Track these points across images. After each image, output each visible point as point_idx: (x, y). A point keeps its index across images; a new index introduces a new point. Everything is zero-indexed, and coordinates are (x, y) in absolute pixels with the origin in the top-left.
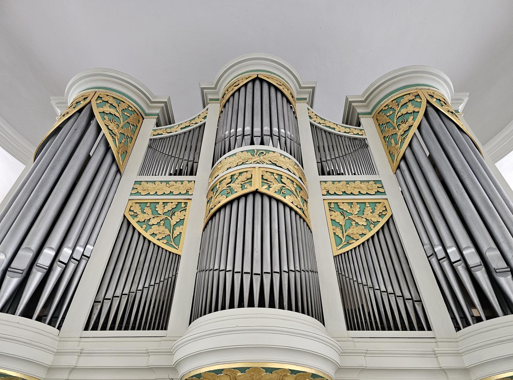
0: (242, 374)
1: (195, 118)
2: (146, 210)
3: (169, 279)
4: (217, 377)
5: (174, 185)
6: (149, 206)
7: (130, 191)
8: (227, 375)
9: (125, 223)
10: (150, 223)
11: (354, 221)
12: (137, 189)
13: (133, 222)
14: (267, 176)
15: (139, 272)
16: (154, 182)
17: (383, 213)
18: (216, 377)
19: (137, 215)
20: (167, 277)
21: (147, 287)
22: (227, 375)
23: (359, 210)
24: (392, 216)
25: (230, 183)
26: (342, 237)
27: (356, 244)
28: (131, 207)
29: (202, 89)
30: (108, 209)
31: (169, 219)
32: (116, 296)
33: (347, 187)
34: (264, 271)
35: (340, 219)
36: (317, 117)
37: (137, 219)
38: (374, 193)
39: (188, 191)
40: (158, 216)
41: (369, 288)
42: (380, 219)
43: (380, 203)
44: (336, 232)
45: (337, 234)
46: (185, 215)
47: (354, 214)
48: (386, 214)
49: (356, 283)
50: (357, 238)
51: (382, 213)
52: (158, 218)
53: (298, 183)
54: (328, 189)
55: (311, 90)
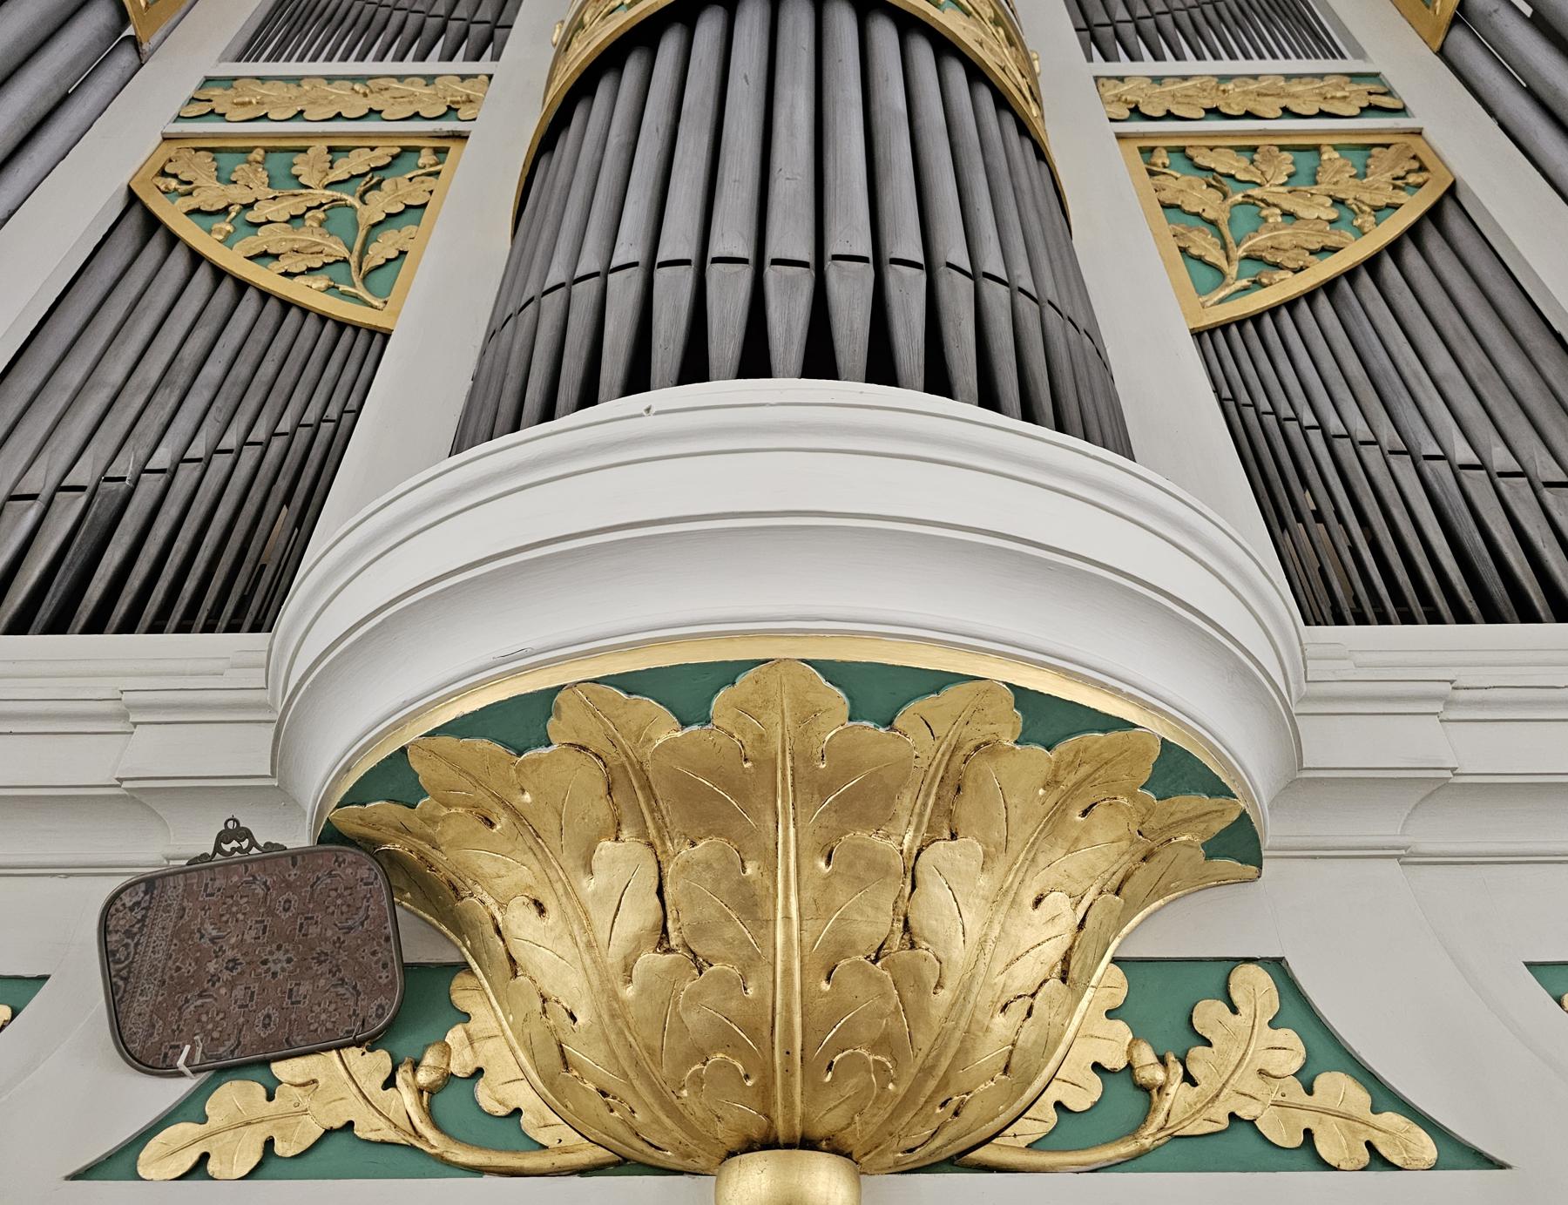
0: (687, 730)
2: (239, 173)
3: (323, 425)
4: (518, 771)
5: (386, 89)
6: (259, 158)
7: (176, 105)
8: (585, 749)
9: (134, 218)
10: (251, 216)
11: (1275, 205)
12: (209, 101)
13: (172, 214)
15: (167, 399)
16: (297, 80)
17: (1412, 179)
18: (513, 773)
19: (194, 189)
20: (311, 416)
21: (198, 456)
22: (585, 749)
23: (1292, 169)
24: (1452, 191)
26: (1223, 263)
28: (171, 161)
30: (53, 163)
31: (352, 207)
32: (25, 492)
33: (1224, 91)
34: (834, 247)
35: (1199, 197)
38: (1357, 111)
39: (453, 106)
40: (296, 192)
41: (1391, 452)
43: (1387, 146)
44: (1190, 244)
45: (1194, 251)
46: (431, 192)
47: (1272, 182)
48: (1425, 182)
49: (1316, 437)
50: (1301, 263)
51: (1403, 178)
52: (298, 199)
54: (1135, 99)
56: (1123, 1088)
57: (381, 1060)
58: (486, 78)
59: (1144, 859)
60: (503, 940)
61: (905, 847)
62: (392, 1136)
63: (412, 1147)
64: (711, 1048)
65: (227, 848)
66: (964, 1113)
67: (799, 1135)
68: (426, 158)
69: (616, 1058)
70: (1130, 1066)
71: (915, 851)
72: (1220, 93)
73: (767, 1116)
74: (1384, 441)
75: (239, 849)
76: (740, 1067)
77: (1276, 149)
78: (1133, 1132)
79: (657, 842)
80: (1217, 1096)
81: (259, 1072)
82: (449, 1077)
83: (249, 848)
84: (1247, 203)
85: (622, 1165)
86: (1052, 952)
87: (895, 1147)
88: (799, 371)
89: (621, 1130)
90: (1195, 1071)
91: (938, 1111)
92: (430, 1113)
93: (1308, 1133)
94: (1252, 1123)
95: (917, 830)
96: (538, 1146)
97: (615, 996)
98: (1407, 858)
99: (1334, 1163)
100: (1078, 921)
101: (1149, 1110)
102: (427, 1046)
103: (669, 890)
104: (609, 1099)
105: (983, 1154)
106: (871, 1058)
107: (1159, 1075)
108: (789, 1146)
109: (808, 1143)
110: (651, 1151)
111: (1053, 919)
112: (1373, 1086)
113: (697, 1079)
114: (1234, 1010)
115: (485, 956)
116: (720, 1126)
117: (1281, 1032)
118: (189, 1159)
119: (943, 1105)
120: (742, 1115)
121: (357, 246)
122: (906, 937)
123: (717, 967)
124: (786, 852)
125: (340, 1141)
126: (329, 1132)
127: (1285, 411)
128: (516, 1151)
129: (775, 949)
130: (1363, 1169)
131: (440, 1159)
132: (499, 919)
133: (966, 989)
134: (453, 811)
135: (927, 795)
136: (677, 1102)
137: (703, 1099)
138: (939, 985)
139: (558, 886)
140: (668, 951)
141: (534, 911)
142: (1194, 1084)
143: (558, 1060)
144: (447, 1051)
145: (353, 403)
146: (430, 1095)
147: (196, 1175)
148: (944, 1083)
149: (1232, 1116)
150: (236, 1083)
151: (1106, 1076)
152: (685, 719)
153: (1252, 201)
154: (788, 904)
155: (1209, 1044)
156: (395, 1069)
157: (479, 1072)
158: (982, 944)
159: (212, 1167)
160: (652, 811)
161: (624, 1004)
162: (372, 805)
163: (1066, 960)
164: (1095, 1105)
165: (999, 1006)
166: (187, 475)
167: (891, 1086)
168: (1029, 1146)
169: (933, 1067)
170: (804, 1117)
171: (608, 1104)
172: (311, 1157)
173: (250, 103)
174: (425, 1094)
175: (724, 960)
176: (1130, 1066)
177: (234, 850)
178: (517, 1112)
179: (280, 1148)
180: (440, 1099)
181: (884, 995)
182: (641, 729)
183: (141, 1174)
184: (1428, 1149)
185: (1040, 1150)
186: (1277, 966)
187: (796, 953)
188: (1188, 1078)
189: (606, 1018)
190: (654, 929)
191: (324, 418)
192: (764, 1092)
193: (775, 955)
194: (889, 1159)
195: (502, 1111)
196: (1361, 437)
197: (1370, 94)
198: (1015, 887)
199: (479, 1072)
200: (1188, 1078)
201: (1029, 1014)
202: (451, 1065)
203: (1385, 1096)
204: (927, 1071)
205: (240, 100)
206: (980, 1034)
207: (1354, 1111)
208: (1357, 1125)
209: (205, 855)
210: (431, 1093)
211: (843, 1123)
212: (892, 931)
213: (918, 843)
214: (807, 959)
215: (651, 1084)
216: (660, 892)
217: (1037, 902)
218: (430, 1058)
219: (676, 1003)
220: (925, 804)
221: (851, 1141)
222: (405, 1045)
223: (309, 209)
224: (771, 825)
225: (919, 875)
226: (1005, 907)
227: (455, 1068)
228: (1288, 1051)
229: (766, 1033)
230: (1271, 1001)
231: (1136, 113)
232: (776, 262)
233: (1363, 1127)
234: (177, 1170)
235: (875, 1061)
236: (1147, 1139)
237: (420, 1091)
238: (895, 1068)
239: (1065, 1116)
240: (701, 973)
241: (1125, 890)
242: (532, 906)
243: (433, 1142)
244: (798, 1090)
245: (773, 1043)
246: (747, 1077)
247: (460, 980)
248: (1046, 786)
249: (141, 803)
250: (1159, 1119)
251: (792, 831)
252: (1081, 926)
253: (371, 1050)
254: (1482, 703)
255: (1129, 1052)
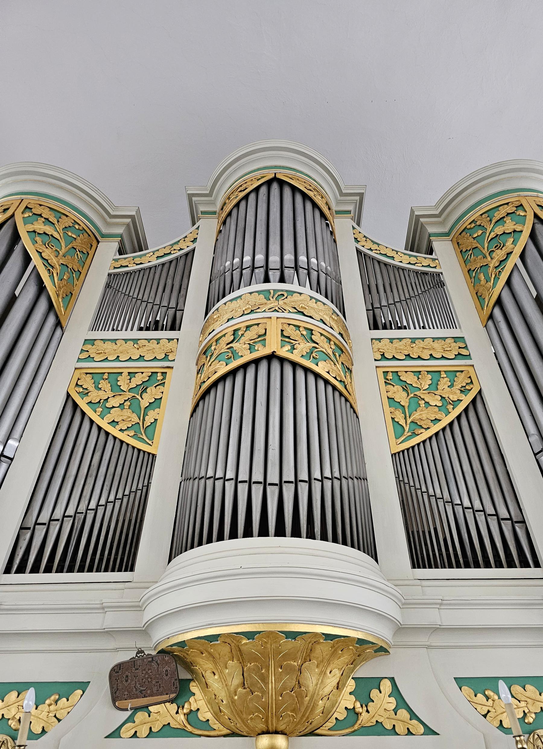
1: (179, 241)
6: (107, 377)
9: (70, 404)
12: (88, 351)
13: (82, 403)
14: (290, 331)
15: (90, 481)
16: (115, 341)
22: (226, 643)
24: (480, 392)
25: (232, 342)
26: (404, 425)
27: (426, 435)
29: (190, 196)
33: (412, 347)
36: (367, 240)
37: (87, 399)
42: (462, 397)
43: (462, 371)
45: (396, 420)
46: (162, 393)
47: (423, 389)
48: (472, 389)
49: (425, 496)
50: (428, 426)
51: (465, 387)
53: (337, 342)
54: (383, 351)
55: (358, 198)
56: (352, 713)
57: (174, 707)
58: (176, 340)
59: (358, 656)
60: (204, 679)
61: (299, 664)
62: (179, 727)
63: (184, 729)
64: (255, 712)
65: (138, 655)
66: (312, 724)
67: (274, 731)
68: (160, 377)
69: (233, 712)
70: (354, 708)
71: (301, 665)
72: (411, 348)
73: (267, 727)
74: (445, 498)
75: (141, 656)
76: (261, 716)
77: (426, 373)
78: (353, 726)
79: (242, 663)
80: (374, 716)
81: (145, 709)
82: (191, 711)
83: (144, 655)
84: (415, 397)
85: (233, 734)
86: (334, 683)
87: (296, 732)
88: (274, 536)
89: (234, 727)
90: (369, 709)
91: (306, 724)
92: (187, 720)
93: (394, 726)
94: (381, 723)
95: (301, 660)
96: (213, 729)
97: (233, 698)
98: (428, 647)
99: (399, 733)
100: (341, 674)
101: (358, 719)
102: (185, 702)
103: (245, 674)
104: (231, 721)
105: (318, 731)
106: (291, 714)
107: (361, 710)
108: (272, 733)
109: (276, 732)
110: (241, 732)
111: (334, 676)
112: (411, 713)
113: (251, 719)
114: (380, 692)
115: (199, 681)
116: (257, 728)
117: (391, 698)
118: (132, 732)
119: (308, 722)
120: (262, 726)
121: (142, 418)
122: (299, 685)
123: (256, 693)
124: (272, 666)
125: (167, 727)
126: (164, 725)
127: (418, 486)
128: (208, 731)
129: (269, 689)
130: (406, 735)
131: (191, 732)
132: (203, 673)
133: (312, 696)
134: (194, 650)
135: (304, 652)
136: (247, 723)
137: (253, 723)
138: (306, 696)
139: (219, 670)
140: (244, 688)
141: (213, 675)
142: (369, 713)
143: (219, 710)
144: (190, 704)
145: (146, 483)
146: (187, 715)
147: (134, 736)
148: (308, 718)
149: (377, 721)
150: (141, 712)
151: (348, 710)
152: (248, 638)
153: (416, 396)
154: (272, 679)
155: (373, 702)
156: (178, 708)
157: (198, 709)
158: (317, 685)
159: (138, 734)
160: (241, 656)
161: (235, 700)
162: (174, 647)
163: (338, 683)
164: (345, 718)
165: (321, 699)
166: (101, 511)
167: (295, 720)
168: (329, 729)
169: (305, 715)
170: (276, 727)
171: (231, 722)
172: (160, 732)
173: (101, 353)
174: (186, 715)
175: (258, 692)
176: (354, 708)
177: (140, 656)
178: (208, 720)
179: (153, 730)
180: (189, 716)
181: (294, 700)
182: (239, 640)
183: (122, 736)
184: (422, 729)
185: (331, 730)
186: (392, 680)
187: (274, 691)
188: (368, 711)
189: (230, 703)
190: (242, 683)
191: (138, 489)
192: (267, 722)
193: (269, 691)
194: (295, 734)
195: (204, 720)
196: (438, 496)
197: (460, 348)
198: (325, 670)
199: (198, 709)
200: (368, 711)
201: (328, 699)
202: (192, 707)
203: (413, 716)
204: (307, 707)
205: (98, 352)
206: (316, 706)
207: (405, 720)
208: (406, 723)
209: (133, 657)
210: (187, 715)
211: (284, 728)
212: (295, 684)
213: (302, 663)
214: (276, 692)
215: (241, 719)
216: (243, 675)
217: (330, 672)
218: (186, 706)
219: (247, 701)
220: (303, 654)
221: (286, 731)
222: (180, 701)
223: (125, 401)
224: (268, 660)
225: (302, 671)
226: (322, 676)
227: (192, 709)
228: (392, 703)
229: (267, 708)
230: (390, 690)
231: (383, 357)
232: (270, 484)
233: (407, 724)
234: (130, 735)
235: (291, 715)
236: (356, 727)
237: (185, 715)
238: (296, 716)
239: (337, 721)
240: (252, 694)
241: (354, 663)
242: (212, 674)
243: (189, 728)
244: (274, 722)
245: (269, 711)
246: (263, 718)
247: (192, 684)
248: (331, 647)
249: (110, 634)
250: (359, 722)
251: (273, 662)
252: (342, 675)
253: (172, 703)
254: (450, 604)
255: (354, 704)
